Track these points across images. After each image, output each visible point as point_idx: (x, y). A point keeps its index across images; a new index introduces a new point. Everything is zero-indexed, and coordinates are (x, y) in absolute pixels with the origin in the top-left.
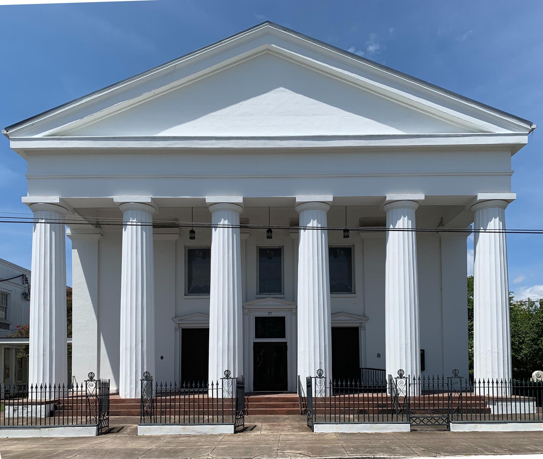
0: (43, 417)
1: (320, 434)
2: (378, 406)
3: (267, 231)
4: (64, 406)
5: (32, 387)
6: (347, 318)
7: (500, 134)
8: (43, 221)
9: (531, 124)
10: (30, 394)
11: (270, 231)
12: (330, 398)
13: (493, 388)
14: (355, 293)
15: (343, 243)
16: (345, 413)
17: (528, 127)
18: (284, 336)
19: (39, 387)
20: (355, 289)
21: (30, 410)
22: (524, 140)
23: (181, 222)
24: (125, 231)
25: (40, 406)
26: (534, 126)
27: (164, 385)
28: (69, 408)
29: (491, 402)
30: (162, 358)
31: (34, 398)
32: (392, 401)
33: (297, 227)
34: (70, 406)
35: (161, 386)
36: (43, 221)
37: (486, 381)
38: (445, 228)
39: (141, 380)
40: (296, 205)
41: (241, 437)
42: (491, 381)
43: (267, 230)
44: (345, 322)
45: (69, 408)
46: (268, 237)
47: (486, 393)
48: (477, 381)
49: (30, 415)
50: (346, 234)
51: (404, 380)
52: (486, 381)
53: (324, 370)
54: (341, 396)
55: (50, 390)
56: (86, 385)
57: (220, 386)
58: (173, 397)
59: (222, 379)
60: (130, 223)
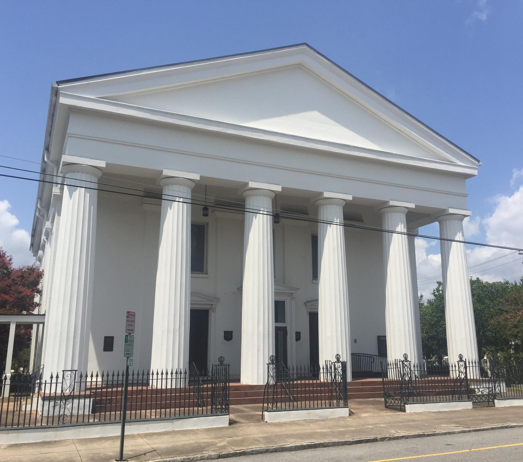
1: (411, 414)
4: (101, 400)
5: (153, 374)
6: (202, 299)
7: (461, 166)
8: (181, 200)
9: (479, 161)
10: (451, 372)
11: (206, 209)
12: (274, 386)
14: (207, 274)
16: (199, 406)
17: (477, 163)
19: (174, 372)
20: (207, 269)
21: (82, 404)
22: (475, 172)
24: (256, 218)
26: (481, 163)
27: (111, 374)
28: (108, 402)
29: (472, 383)
31: (48, 391)
32: (268, 391)
33: (243, 209)
34: (109, 399)
35: (138, 375)
36: (181, 200)
37: (160, 373)
38: (365, 225)
39: (268, 364)
40: (162, 177)
41: (350, 419)
42: (164, 373)
43: (203, 207)
45: (108, 402)
49: (81, 412)
50: (205, 213)
52: (160, 373)
53: (340, 354)
55: (57, 380)
57: (60, 380)
59: (268, 364)
60: (261, 212)
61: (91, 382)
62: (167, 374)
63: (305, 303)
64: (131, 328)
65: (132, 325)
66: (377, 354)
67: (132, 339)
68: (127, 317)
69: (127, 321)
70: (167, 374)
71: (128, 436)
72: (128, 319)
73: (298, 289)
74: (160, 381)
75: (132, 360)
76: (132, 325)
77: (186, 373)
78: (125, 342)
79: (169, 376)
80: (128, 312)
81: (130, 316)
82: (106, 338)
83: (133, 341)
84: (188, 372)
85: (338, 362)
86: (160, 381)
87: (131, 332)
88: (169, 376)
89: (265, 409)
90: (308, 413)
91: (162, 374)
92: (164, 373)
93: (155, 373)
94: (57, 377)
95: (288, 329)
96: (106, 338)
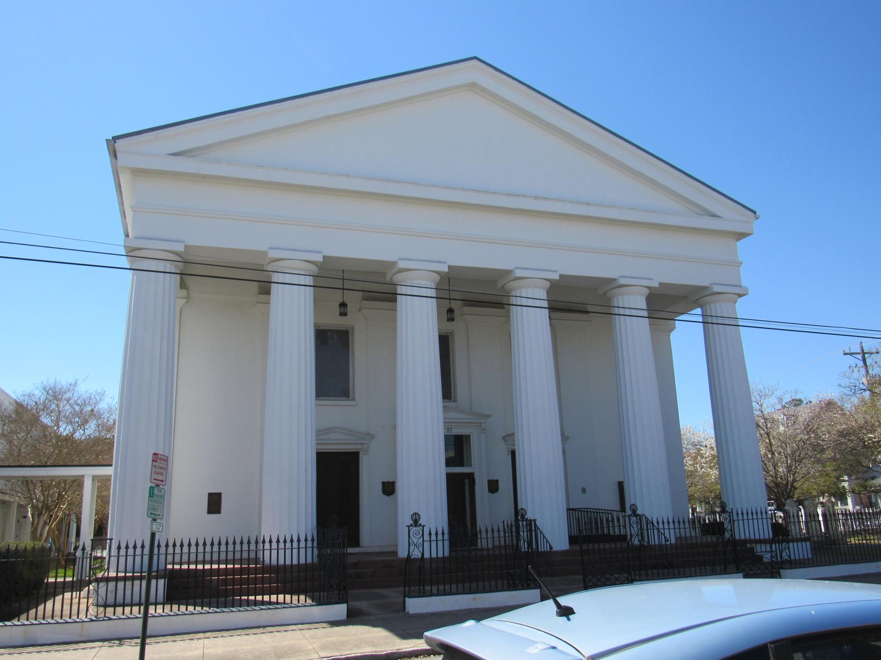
0: (810, 556)
2: (263, 580)
3: (448, 311)
13: (126, 557)
15: (334, 321)
18: (470, 465)
23: (590, 308)
25: (114, 583)
30: (584, 490)
37: (131, 546)
39: (409, 527)
44: (338, 444)
46: (449, 320)
47: (747, 535)
48: (483, 530)
51: (419, 529)
54: (232, 566)
55: (143, 551)
56: (423, 534)
58: (230, 566)
59: (409, 527)
61: (204, 552)
62: (299, 541)
63: (504, 438)
64: (160, 477)
65: (157, 473)
66: (619, 509)
67: (162, 494)
68: (153, 461)
69: (153, 466)
70: (299, 541)
71: (138, 638)
72: (155, 463)
73: (489, 416)
74: (281, 552)
75: (161, 525)
76: (162, 474)
77: (313, 540)
78: (150, 496)
79: (302, 544)
80: (155, 454)
81: (621, 485)
82: (211, 495)
83: (163, 497)
84: (315, 538)
85: (416, 526)
86: (281, 552)
87: (160, 483)
88: (302, 544)
89: (407, 594)
90: (475, 599)
91: (135, 547)
92: (295, 539)
93: (163, 545)
94: (143, 547)
95: (477, 477)
96: (211, 495)
